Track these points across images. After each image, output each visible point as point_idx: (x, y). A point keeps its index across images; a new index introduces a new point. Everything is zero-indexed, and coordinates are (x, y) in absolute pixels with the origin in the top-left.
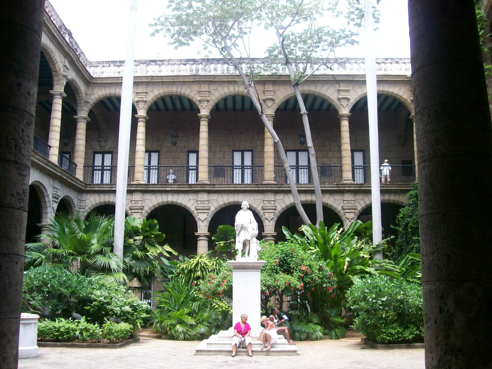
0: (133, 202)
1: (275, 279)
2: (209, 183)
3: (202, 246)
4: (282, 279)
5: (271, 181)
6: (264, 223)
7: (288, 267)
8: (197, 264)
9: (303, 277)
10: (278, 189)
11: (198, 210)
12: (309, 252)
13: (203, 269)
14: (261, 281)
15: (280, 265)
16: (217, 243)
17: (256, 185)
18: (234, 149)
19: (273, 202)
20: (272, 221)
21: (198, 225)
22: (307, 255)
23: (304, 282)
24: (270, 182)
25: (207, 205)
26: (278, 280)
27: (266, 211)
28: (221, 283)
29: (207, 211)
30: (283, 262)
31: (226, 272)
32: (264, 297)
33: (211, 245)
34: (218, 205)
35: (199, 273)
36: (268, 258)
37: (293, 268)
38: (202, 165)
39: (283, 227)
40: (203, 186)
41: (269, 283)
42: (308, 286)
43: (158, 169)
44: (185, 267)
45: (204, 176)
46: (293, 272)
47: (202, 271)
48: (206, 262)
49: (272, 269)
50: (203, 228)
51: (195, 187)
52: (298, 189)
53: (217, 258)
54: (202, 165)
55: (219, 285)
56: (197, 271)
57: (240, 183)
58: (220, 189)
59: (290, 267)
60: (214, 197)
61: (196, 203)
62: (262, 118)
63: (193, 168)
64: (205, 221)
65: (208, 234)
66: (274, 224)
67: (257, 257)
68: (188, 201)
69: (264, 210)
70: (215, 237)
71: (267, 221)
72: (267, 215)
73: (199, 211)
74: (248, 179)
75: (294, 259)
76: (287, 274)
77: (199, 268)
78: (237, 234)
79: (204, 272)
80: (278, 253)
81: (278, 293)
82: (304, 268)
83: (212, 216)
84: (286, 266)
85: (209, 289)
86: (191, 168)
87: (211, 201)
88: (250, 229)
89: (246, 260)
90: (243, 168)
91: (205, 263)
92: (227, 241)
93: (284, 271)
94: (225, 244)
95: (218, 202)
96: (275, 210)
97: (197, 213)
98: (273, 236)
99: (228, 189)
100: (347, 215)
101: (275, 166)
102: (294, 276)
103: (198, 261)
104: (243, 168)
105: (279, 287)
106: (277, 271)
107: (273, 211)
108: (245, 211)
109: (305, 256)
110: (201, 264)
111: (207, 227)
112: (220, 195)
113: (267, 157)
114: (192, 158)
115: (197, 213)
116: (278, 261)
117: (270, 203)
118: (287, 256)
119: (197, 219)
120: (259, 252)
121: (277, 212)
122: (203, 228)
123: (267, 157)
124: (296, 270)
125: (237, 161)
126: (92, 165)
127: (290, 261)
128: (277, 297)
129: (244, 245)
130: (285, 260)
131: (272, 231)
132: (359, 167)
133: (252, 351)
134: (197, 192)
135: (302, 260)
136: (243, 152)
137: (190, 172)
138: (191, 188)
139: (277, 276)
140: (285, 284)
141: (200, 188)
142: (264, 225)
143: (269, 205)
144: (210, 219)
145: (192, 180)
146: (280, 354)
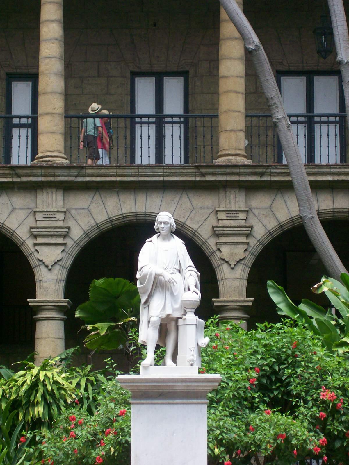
0: (39, 216)
1: (247, 424)
2: (66, 162)
3: (49, 337)
4: (267, 426)
7: (283, 394)
8: (34, 386)
9: (326, 419)
11: (35, 237)
12: (341, 351)
13: (52, 398)
14: (210, 431)
15: (262, 388)
16: (89, 327)
17: (197, 167)
18: (136, 70)
19: (242, 216)
20: (240, 267)
21: (37, 278)
22: (337, 358)
23: (329, 435)
24: (234, 160)
25: (60, 224)
26: (255, 429)
27: (223, 239)
28: (100, 436)
29: (60, 240)
30: (269, 378)
31: (112, 405)
33: (73, 333)
34: (93, 223)
35: (40, 410)
36: (229, 366)
37: (298, 396)
38: (47, 114)
39: (269, 282)
40: (51, 171)
41: (232, 436)
42: (338, 444)
43: (186, 123)
45: (52, 143)
46: (297, 406)
47: (48, 405)
50: (50, 287)
51: (28, 175)
52: (312, 178)
53: (89, 367)
54: (47, 114)
55: (93, 442)
56: (34, 405)
57: (153, 162)
58: (99, 179)
59: (289, 393)
60: (80, 201)
61: (31, 219)
63: (24, 121)
64: (57, 267)
65: (64, 302)
66: (246, 276)
67: (196, 367)
69: (218, 236)
70: (83, 310)
71: (225, 266)
72: (226, 251)
73: (40, 240)
74: (174, 154)
76: (282, 412)
77: (39, 395)
79: (55, 408)
80: (255, 353)
82: (326, 395)
83: (75, 253)
84: (278, 388)
86: (16, 121)
87: (73, 212)
88: (178, 288)
89: (169, 371)
90: (160, 121)
91: (56, 383)
92: (116, 320)
93: (273, 404)
94: (110, 329)
95: (91, 214)
96: (248, 236)
99: (119, 179)
100: (226, 251)
101: (247, 116)
102: (301, 417)
103: (37, 376)
104: (160, 121)
106: (252, 403)
107: (243, 239)
108: (166, 238)
109: (331, 363)
110: (45, 385)
111: (62, 284)
112: (97, 194)
113: (226, 92)
114: (21, 93)
115: (35, 245)
116: (254, 375)
117: (236, 218)
118: (280, 362)
119: (33, 262)
121: (253, 242)
122: (50, 287)
123: (226, 92)
124: (306, 402)
125: (145, 104)
126: (127, 113)
127: (290, 376)
130: (275, 372)
131: (241, 294)
132: (327, 119)
134: (33, 188)
135: (323, 372)
136: (159, 78)
137: (15, 132)
138: (19, 176)
140: (275, 440)
141: (42, 175)
143: (233, 223)
144: (69, 263)
145: (20, 155)
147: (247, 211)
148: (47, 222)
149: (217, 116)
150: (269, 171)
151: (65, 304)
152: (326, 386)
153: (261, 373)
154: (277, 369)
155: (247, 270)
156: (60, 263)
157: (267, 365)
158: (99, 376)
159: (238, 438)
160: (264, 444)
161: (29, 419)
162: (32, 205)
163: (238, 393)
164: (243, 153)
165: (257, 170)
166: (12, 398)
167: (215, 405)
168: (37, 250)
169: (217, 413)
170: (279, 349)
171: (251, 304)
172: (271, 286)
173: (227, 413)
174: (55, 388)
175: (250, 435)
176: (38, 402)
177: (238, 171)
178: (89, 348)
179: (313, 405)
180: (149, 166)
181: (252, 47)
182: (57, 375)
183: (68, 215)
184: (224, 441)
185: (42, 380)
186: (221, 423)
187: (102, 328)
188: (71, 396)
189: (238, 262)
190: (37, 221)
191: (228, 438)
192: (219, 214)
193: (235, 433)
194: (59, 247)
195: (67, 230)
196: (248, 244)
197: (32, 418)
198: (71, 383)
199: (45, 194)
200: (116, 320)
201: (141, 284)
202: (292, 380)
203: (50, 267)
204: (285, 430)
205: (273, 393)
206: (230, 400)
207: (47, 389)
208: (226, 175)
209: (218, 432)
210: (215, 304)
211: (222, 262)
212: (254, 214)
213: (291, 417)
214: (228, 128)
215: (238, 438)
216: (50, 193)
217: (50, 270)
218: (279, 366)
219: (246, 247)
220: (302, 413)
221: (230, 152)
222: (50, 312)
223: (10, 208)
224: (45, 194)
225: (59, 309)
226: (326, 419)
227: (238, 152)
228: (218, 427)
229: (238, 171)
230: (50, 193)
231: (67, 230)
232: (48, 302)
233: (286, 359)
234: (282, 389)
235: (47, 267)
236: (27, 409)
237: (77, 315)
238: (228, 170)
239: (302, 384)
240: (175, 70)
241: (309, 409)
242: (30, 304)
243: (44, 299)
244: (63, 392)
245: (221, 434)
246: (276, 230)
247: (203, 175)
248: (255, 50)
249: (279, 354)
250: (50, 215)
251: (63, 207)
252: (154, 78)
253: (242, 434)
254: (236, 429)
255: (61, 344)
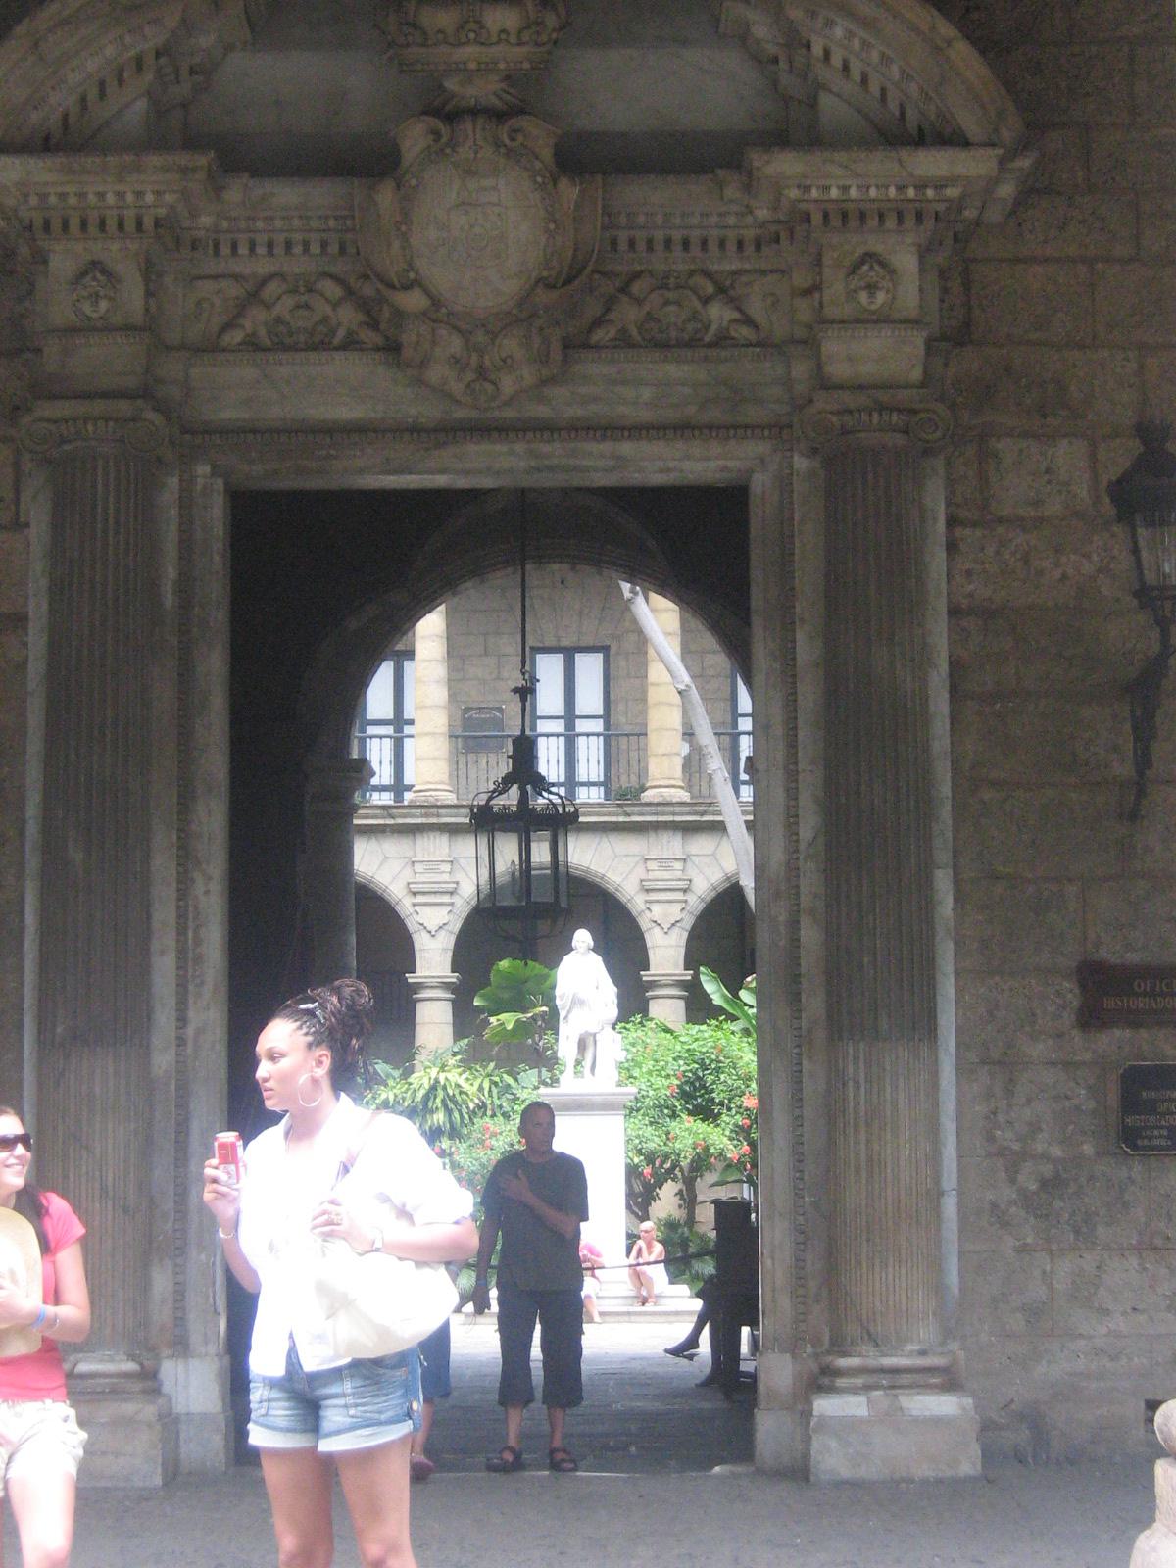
0: (419, 868)
3: (434, 1021)
4: (686, 1134)
5: (673, 790)
6: (646, 936)
8: (433, 1088)
9: (750, 1127)
10: (697, 818)
11: (415, 894)
14: (629, 1141)
15: (686, 1096)
16: (493, 1020)
19: (678, 866)
20: (676, 930)
21: (417, 945)
25: (446, 877)
26: (676, 1138)
27: (654, 896)
29: (446, 899)
30: (692, 1083)
32: (638, 1188)
33: (465, 1020)
36: (650, 1073)
37: (721, 1104)
39: (701, 969)
40: (434, 811)
41: (651, 1145)
44: (391, 1098)
46: (720, 1114)
47: (449, 1112)
48: (461, 1081)
49: (660, 1108)
50: (433, 958)
51: (404, 816)
56: (432, 1112)
61: (408, 872)
62: (633, 607)
64: (443, 933)
65: (453, 978)
67: (616, 1077)
68: (381, 864)
70: (483, 996)
71: (657, 930)
73: (420, 899)
75: (722, 1077)
76: (703, 1120)
77: (438, 1100)
78: (561, 1017)
79: (456, 1115)
81: (679, 1175)
83: (464, 915)
85: (483, 1166)
87: (462, 861)
91: (458, 1086)
96: (685, 891)
97: (414, 905)
98: (446, 986)
100: (657, 911)
102: (723, 1125)
103: (437, 1081)
105: (679, 1155)
106: (674, 1112)
107: (679, 896)
110: (444, 1088)
111: (450, 954)
113: (659, 703)
115: (414, 905)
117: (668, 869)
119: (411, 925)
120: (620, 1067)
121: (692, 899)
122: (433, 958)
123: (659, 703)
124: (729, 1109)
127: (714, 1082)
128: (680, 1185)
129: (582, 1045)
130: (699, 1079)
131: (676, 966)
133: (602, 1314)
136: (569, 653)
138: (392, 817)
139: (674, 1126)
141: (422, 816)
142: (649, 944)
143: (666, 875)
144: (457, 926)
146: (672, 1318)
147: (685, 860)
148: (427, 875)
149: (646, 734)
150: (711, 809)
151: (454, 980)
152: (750, 1092)
153: (683, 1080)
154: (701, 1074)
155: (685, 935)
156: (446, 927)
157: (691, 1071)
158: (505, 1076)
159: (658, 1147)
160: (683, 1153)
161: (427, 1128)
162: (409, 853)
163: (659, 1103)
164: (681, 784)
165: (696, 808)
166: (406, 1104)
167: (635, 1114)
168: (416, 911)
169: (637, 1121)
170: (704, 1053)
171: (689, 978)
172: (703, 974)
173: (647, 1122)
174: (457, 1092)
175: (671, 1144)
176: (437, 1108)
177: (672, 809)
178: (490, 1040)
179: (737, 1113)
180: (384, 807)
181: (682, 687)
182: (455, 1077)
183: (455, 866)
184: (643, 1151)
185: (442, 1083)
186: (641, 1132)
187: (508, 1022)
188: (472, 1100)
189: (673, 925)
190: (415, 873)
191: (647, 1147)
192: (649, 863)
193: (654, 1142)
194: (444, 907)
195: (455, 885)
196: (686, 901)
197: (431, 1128)
198: (472, 1084)
199: (426, 839)
200: (524, 1011)
201: (561, 1000)
202: (715, 1086)
203: (433, 933)
204: (704, 1139)
205: (696, 1099)
206: (648, 1108)
207: (448, 1095)
208: (656, 814)
209: (637, 1141)
210: (644, 979)
211: (653, 925)
212: (694, 863)
213: (712, 1125)
214: (661, 751)
215: (658, 1147)
216: (432, 838)
217: (433, 936)
218: (703, 1071)
219: (684, 905)
220: (724, 1122)
221: (661, 783)
222: (435, 991)
223: (381, 858)
224: (426, 839)
225: (446, 986)
226: (750, 1127)
227: (673, 782)
228: (638, 1137)
229: (672, 809)
230: (432, 838)
231: (455, 885)
232: (433, 977)
233: (710, 1065)
234: (706, 1096)
235: (430, 932)
236: (424, 1117)
237: (476, 1003)
238: (659, 808)
239: (726, 1091)
240: (591, 644)
241: (733, 1117)
242: (410, 980)
243: (427, 974)
244: (464, 1096)
245: (640, 1143)
246: (722, 882)
247: (629, 815)
248: (685, 690)
249: (703, 1059)
250: (432, 865)
251: (449, 856)
252: (562, 655)
253: (662, 1143)
254: (656, 1139)
255: (449, 1030)
